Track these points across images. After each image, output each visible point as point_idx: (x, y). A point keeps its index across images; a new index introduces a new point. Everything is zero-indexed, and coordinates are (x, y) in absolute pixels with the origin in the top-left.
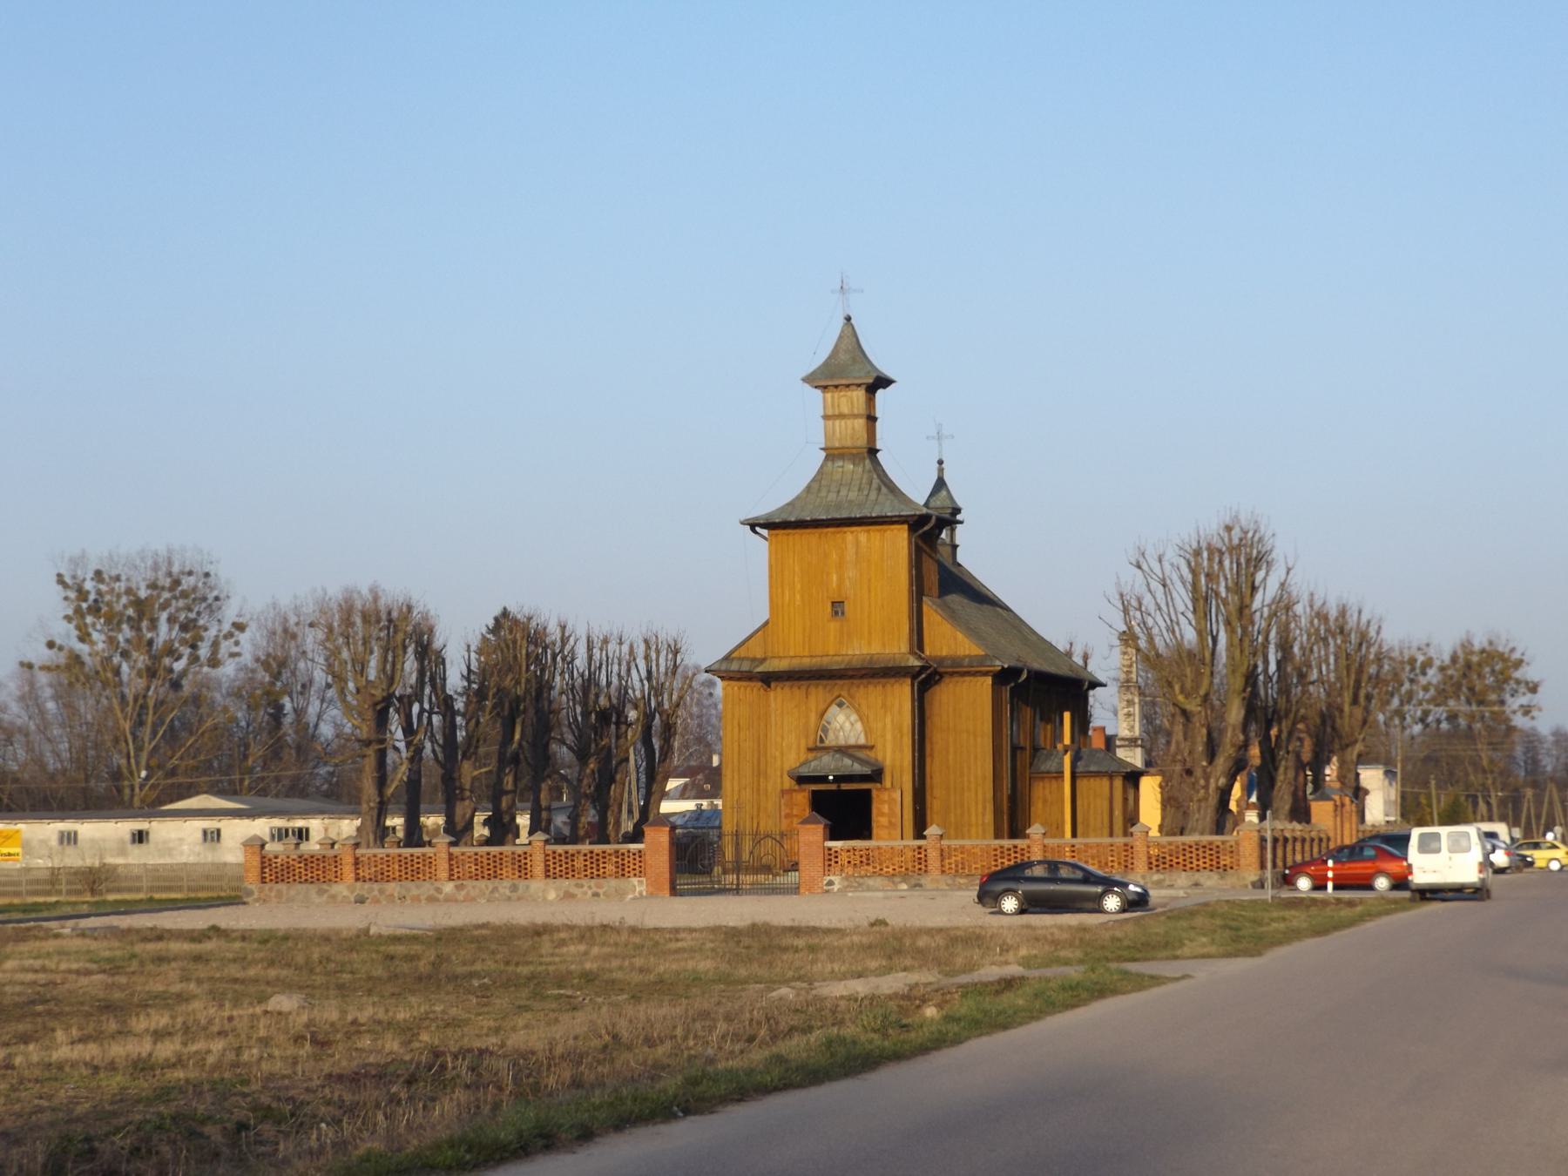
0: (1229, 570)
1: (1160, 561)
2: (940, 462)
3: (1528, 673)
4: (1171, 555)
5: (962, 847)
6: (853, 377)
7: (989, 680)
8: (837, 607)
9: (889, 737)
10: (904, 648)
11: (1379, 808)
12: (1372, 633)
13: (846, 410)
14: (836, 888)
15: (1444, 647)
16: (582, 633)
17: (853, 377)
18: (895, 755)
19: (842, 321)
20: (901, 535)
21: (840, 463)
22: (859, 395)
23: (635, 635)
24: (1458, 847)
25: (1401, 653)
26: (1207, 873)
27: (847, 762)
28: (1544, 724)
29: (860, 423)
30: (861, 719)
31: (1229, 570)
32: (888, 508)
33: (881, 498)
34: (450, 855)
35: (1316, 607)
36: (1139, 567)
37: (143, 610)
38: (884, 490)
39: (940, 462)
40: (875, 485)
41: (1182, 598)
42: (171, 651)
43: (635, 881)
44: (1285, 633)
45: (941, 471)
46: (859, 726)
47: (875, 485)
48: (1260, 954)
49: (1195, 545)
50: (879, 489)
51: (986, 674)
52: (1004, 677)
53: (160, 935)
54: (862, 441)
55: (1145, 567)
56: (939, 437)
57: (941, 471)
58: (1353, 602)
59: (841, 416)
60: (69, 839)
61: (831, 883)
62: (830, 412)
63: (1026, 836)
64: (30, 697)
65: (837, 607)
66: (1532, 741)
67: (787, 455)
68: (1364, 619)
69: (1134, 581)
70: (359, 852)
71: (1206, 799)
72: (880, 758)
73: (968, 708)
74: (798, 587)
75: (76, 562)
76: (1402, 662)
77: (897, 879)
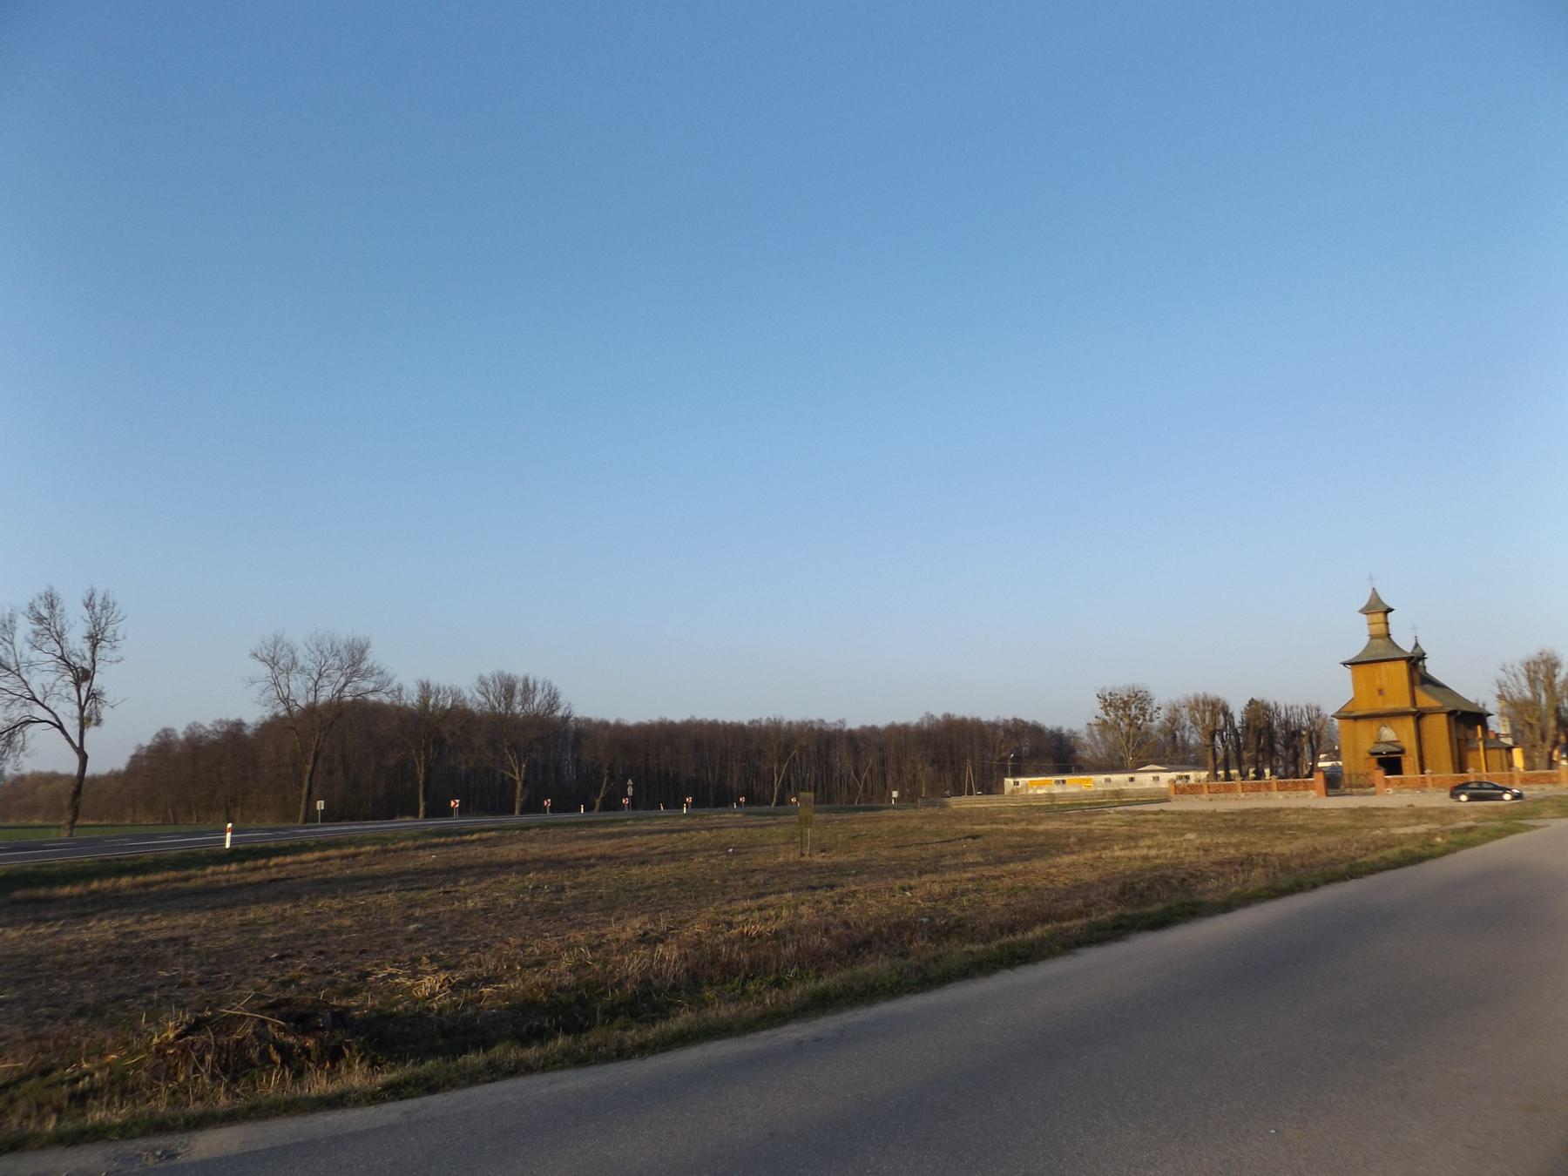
6: (1378, 609)
8: (1381, 692)
17: (1378, 609)
20: (1403, 665)
23: (1302, 704)
37: (1126, 704)
60: (1108, 780)
64: (1091, 734)
65: (1381, 692)
69: (1502, 676)
73: (1438, 727)
75: (1103, 689)
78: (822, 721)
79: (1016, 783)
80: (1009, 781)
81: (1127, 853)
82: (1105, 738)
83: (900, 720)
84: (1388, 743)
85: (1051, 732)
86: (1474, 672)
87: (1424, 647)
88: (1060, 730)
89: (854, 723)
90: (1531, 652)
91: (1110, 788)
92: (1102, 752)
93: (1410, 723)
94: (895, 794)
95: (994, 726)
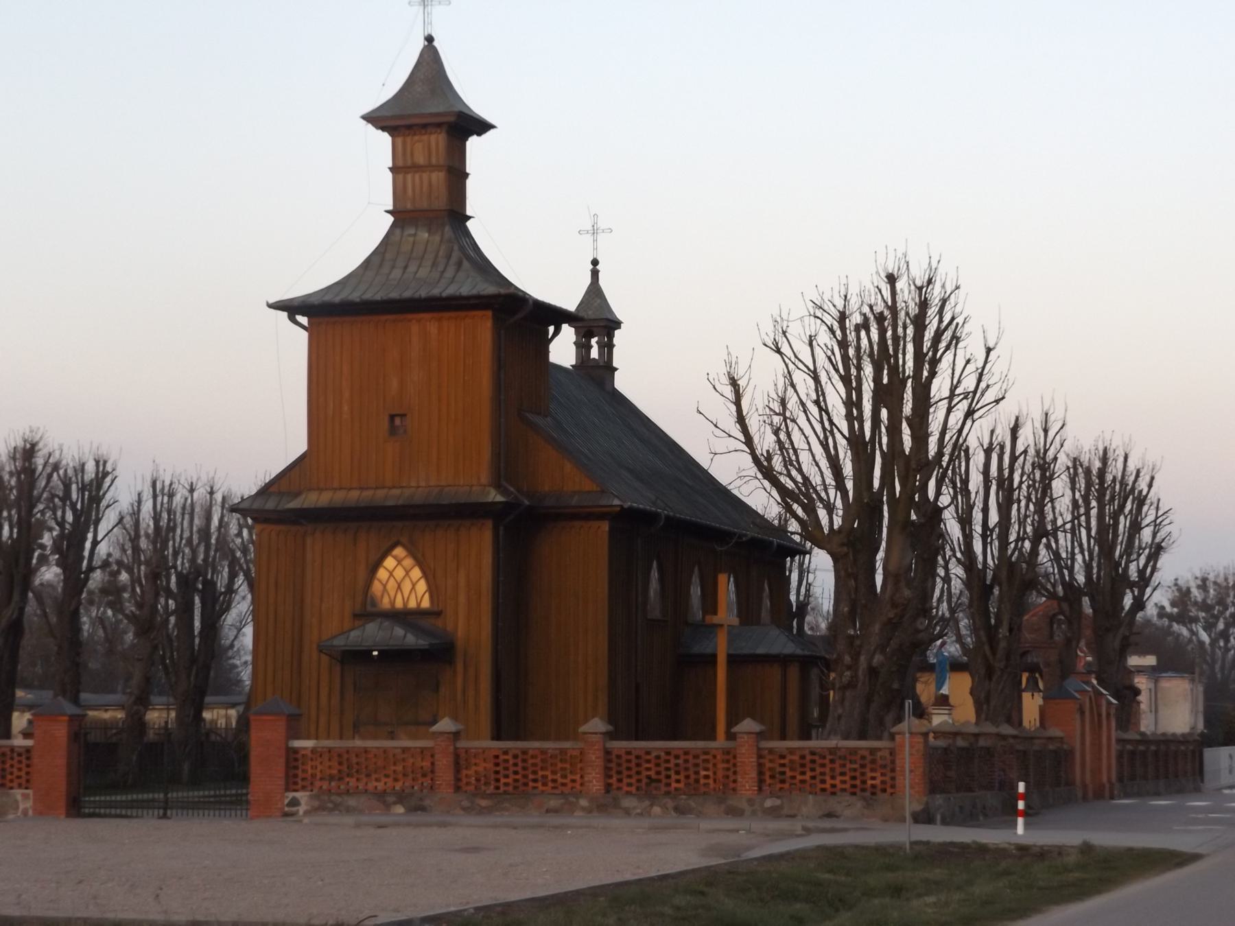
1: (811, 345)
2: (595, 262)
5: (563, 751)
6: (431, 126)
7: (605, 526)
9: (462, 599)
10: (485, 478)
12: (1143, 485)
13: (421, 159)
14: (301, 809)
16: (44, 452)
17: (431, 126)
18: (473, 627)
19: (420, 44)
20: (483, 327)
21: (412, 231)
22: (438, 140)
25: (1226, 579)
26: (847, 798)
27: (399, 631)
29: (439, 178)
30: (425, 575)
31: (895, 350)
32: (468, 285)
33: (461, 275)
34: (608, 752)
35: (1158, 540)
36: (778, 351)
38: (466, 264)
39: (595, 262)
40: (454, 259)
43: (18, 793)
45: (595, 274)
46: (422, 586)
47: (454, 259)
49: (840, 304)
50: (459, 264)
51: (601, 517)
52: (629, 523)
54: (441, 202)
55: (785, 349)
56: (595, 231)
57: (595, 274)
58: (1117, 446)
59: (416, 168)
61: (294, 803)
62: (400, 163)
63: (575, 736)
65: (395, 422)
67: (345, 217)
68: (1132, 467)
70: (462, 744)
71: (851, 685)
72: (450, 628)
73: (580, 565)
74: (347, 394)
76: (1227, 588)
77: (391, 799)
84: (404, 617)
86: (709, 364)
87: (474, 93)
90: (862, 286)
93: (479, 548)
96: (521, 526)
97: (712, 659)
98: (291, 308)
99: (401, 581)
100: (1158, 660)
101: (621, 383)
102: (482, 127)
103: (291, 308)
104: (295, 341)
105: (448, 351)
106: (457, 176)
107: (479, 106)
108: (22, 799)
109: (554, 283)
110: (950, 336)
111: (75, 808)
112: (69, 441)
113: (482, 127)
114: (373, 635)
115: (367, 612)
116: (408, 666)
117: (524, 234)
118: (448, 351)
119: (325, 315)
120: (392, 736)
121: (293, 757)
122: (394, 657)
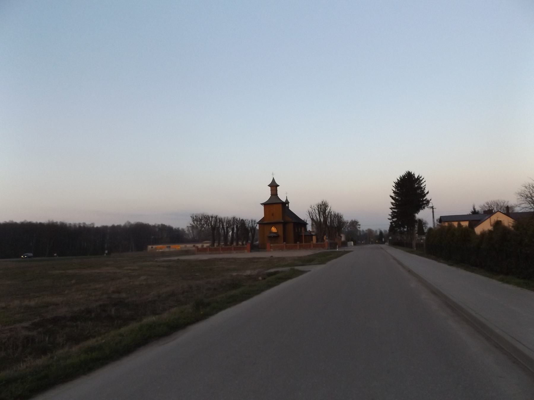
0: (323, 208)
3: (359, 223)
4: (316, 206)
5: (254, 248)
6: (274, 186)
8: (273, 215)
11: (343, 239)
15: (350, 221)
17: (274, 186)
18: (281, 233)
20: (281, 205)
23: (250, 219)
24: (312, 228)
28: (361, 229)
31: (323, 208)
37: (201, 220)
41: (317, 211)
42: (204, 224)
44: (330, 216)
48: (325, 264)
52: (294, 223)
53: (170, 261)
60: (186, 246)
64: (188, 230)
65: (273, 215)
66: (360, 231)
67: (267, 195)
69: (310, 210)
73: (290, 227)
75: (193, 214)
78: (84, 223)
79: (152, 247)
80: (150, 247)
81: (11, 327)
82: (193, 232)
83: (105, 224)
84: (274, 233)
85: (175, 229)
86: (302, 207)
87: (277, 182)
88: (178, 228)
89: (98, 224)
90: (319, 202)
91: (186, 249)
92: (191, 237)
93: (281, 227)
94: (106, 252)
95: (154, 227)
96: (285, 224)
97: (302, 236)
98: (262, 204)
99: (274, 229)
100: (414, 216)
101: (290, 208)
102: (278, 186)
103: (262, 204)
104: (262, 207)
105: (276, 207)
106: (277, 191)
107: (278, 184)
108: (246, 251)
109: (284, 200)
110: (327, 206)
111: (251, 252)
112: (244, 218)
113: (278, 186)
114: (272, 235)
115: (271, 232)
116: (274, 238)
117: (282, 196)
118: (276, 207)
119: (265, 204)
120: (178, 259)
121: (271, 246)
122: (274, 237)
